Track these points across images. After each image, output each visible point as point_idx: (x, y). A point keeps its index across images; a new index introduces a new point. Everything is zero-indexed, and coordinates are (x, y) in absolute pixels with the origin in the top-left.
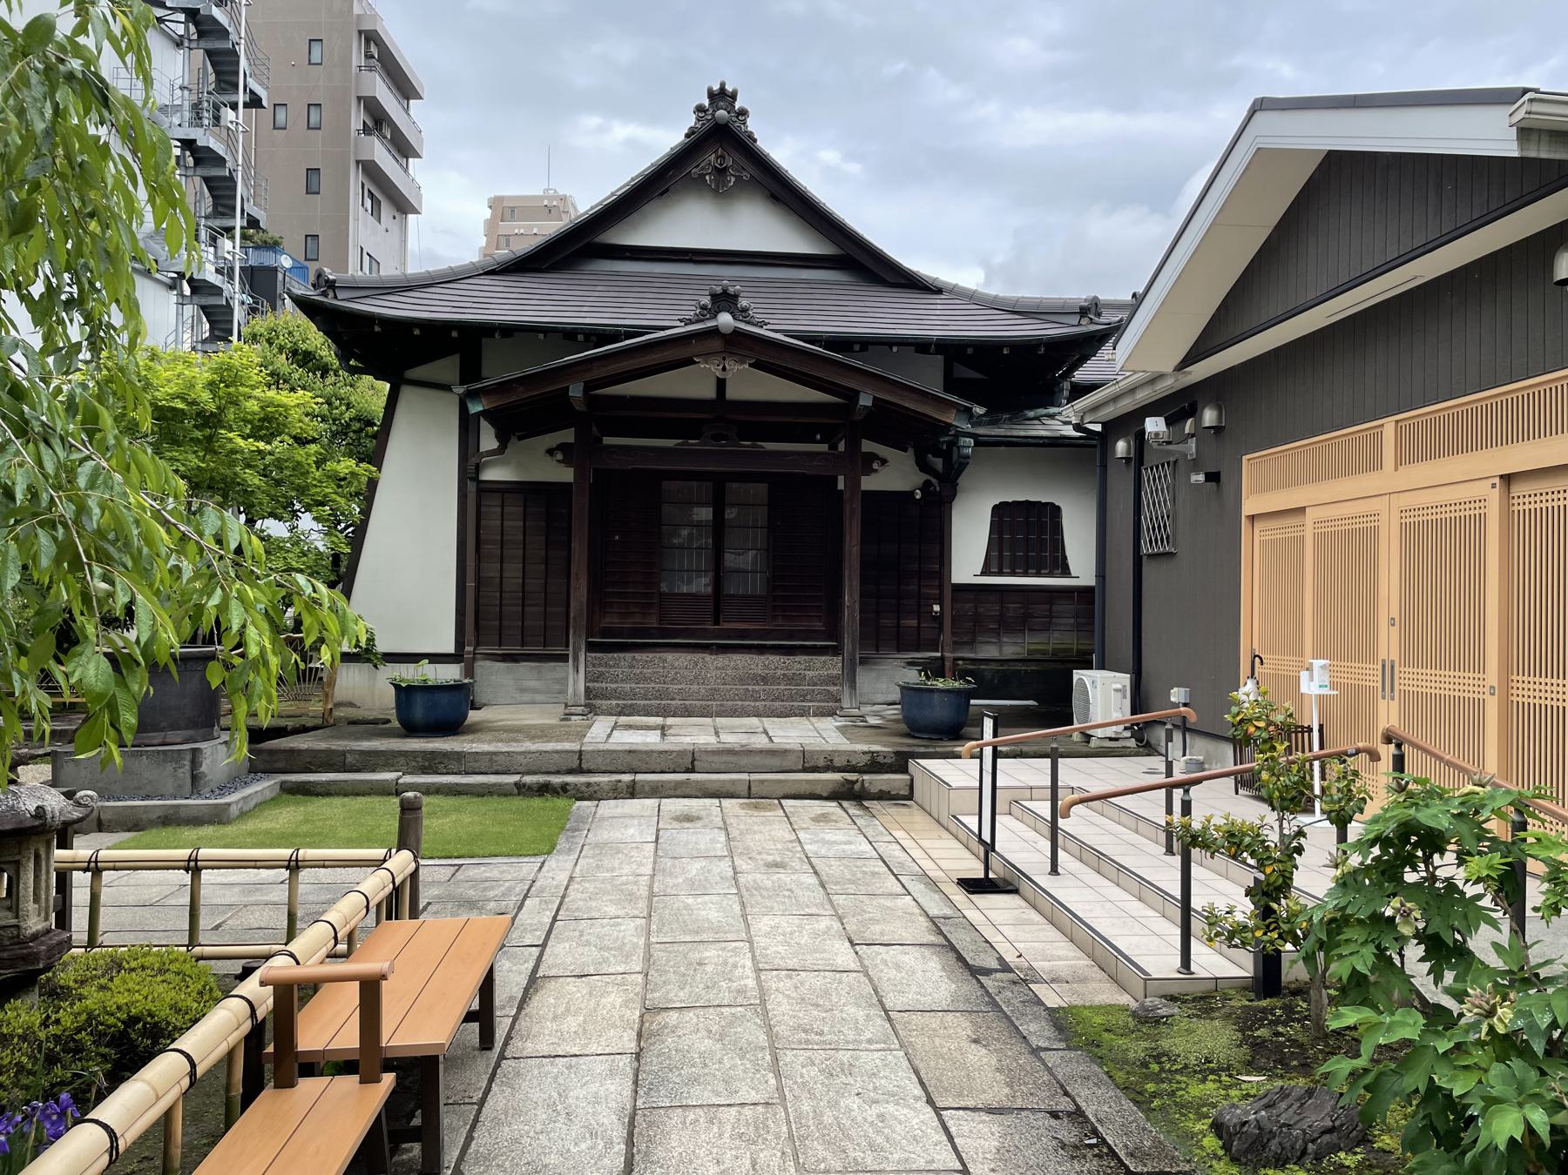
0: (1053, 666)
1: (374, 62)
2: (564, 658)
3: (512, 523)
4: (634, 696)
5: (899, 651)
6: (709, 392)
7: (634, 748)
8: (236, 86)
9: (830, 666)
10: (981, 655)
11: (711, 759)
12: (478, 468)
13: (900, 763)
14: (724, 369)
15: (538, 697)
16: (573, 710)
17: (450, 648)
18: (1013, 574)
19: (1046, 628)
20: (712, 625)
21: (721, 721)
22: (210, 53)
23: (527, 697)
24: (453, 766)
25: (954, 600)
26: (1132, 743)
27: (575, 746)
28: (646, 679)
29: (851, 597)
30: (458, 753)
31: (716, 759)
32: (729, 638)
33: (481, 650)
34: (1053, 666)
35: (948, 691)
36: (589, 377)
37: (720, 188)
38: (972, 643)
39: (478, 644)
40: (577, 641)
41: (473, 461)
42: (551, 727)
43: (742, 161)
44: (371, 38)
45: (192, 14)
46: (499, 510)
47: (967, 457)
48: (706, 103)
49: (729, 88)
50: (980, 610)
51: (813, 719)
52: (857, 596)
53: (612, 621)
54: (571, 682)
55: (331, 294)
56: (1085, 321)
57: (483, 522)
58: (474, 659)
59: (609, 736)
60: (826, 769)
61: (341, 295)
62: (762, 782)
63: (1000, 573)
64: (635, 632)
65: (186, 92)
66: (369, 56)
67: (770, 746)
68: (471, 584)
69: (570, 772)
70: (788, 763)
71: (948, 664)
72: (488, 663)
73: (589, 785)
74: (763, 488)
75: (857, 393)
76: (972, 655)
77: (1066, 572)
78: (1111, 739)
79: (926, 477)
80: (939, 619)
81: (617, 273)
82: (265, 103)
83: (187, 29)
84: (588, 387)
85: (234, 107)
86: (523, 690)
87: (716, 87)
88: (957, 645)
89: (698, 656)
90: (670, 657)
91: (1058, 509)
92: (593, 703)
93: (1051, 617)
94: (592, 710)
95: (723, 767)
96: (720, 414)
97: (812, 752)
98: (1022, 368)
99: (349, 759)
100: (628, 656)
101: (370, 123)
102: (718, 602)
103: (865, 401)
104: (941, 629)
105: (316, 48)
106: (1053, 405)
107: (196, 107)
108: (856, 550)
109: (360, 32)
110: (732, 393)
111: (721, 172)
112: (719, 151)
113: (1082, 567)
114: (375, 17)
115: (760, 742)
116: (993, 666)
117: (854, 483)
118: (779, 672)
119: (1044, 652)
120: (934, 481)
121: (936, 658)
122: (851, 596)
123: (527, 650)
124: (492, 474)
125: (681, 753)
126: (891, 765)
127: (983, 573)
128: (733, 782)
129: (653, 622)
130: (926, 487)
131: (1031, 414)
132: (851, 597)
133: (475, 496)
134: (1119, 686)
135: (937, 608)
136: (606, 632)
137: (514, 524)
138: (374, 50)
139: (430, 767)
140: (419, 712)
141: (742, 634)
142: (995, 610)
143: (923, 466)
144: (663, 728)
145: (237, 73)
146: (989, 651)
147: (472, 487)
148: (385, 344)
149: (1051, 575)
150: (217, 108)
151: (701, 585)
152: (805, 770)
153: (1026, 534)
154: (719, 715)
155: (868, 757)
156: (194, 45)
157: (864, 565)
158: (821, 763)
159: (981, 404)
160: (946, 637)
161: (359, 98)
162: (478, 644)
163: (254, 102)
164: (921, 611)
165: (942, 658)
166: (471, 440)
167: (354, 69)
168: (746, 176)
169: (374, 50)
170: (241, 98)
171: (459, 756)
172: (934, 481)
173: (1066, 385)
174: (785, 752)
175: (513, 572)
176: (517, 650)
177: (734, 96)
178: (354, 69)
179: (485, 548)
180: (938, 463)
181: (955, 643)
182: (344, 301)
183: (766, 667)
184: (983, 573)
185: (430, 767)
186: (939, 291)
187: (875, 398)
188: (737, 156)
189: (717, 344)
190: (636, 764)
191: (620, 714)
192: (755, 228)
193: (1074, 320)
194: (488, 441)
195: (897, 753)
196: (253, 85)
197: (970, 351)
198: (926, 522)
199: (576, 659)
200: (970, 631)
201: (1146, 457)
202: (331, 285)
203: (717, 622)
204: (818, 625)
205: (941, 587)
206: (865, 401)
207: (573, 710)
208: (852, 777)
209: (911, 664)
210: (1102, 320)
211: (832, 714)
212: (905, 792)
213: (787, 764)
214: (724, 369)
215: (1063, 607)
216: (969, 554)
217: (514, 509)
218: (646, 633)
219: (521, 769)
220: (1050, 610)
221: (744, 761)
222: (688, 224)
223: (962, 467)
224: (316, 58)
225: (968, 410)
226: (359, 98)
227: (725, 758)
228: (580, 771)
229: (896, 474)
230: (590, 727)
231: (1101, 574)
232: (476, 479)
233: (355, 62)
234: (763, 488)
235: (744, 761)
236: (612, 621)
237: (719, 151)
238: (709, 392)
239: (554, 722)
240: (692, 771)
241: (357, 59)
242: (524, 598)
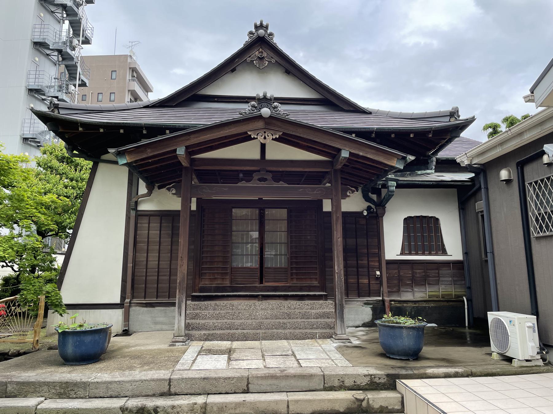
0: (442, 304)
1: (134, 78)
2: (173, 304)
3: (154, 232)
4: (215, 328)
5: (359, 296)
6: (257, 156)
7: (207, 375)
8: (76, 78)
9: (327, 306)
10: (404, 298)
11: (260, 382)
12: (136, 203)
13: (390, 384)
14: (265, 138)
15: (164, 327)
16: (178, 339)
17: (118, 300)
18: (417, 254)
19: (437, 283)
20: (259, 283)
21: (266, 344)
22: (67, 66)
23: (158, 327)
24: (81, 393)
25: (387, 269)
26: (541, 363)
27: (163, 374)
28: (223, 317)
29: (338, 266)
30: (84, 383)
31: (264, 382)
32: (268, 291)
33: (135, 301)
34: (442, 304)
35: (412, 328)
36: (188, 143)
37: (260, 68)
38: (398, 291)
39: (133, 297)
40: (179, 296)
41: (134, 200)
42: (160, 352)
43: (272, 54)
44: (134, 70)
45: (60, 51)
46: (147, 225)
47: (393, 191)
48: (254, 31)
49: (265, 24)
50: (401, 274)
51: (319, 341)
52: (342, 266)
53: (205, 283)
54: (176, 321)
55: (56, 111)
56: (452, 119)
57: (138, 232)
58: (130, 306)
59: (194, 361)
60: (342, 387)
61: (62, 112)
62: (297, 401)
63: (410, 254)
64: (217, 289)
65: (56, 80)
66: (133, 76)
67: (299, 371)
68: (130, 265)
69: (162, 395)
70: (314, 384)
71: (387, 304)
72: (138, 308)
73: (173, 407)
74: (283, 213)
75: (339, 150)
76: (399, 299)
77: (444, 252)
78: (527, 361)
79: (368, 204)
80: (379, 279)
81: (211, 108)
82: (87, 85)
83: (58, 58)
84: (191, 151)
85: (75, 86)
86: (156, 323)
87: (258, 23)
88: (390, 293)
89: (251, 302)
90: (236, 302)
91: (437, 220)
92: (189, 334)
93: (439, 277)
94: (189, 338)
95: (269, 389)
96: (263, 167)
97: (330, 376)
98: (424, 141)
99: (10, 388)
100: (213, 303)
101: (133, 99)
102: (262, 271)
103: (345, 154)
104: (381, 284)
105: (114, 74)
106: (428, 169)
107: (60, 87)
108: (340, 240)
109: (130, 68)
110: (269, 156)
111: (261, 59)
112: (260, 51)
113: (454, 249)
114: (135, 63)
115: (291, 366)
116: (410, 304)
117: (336, 205)
118: (297, 311)
119: (437, 296)
120: (373, 206)
121: (380, 301)
122: (338, 266)
123: (160, 300)
124: (145, 206)
125: (240, 379)
126: (384, 384)
127: (402, 254)
128: (277, 402)
129: (227, 283)
130: (369, 209)
131: (419, 172)
132: (338, 266)
133: (135, 217)
134: (531, 325)
135: (378, 273)
136: (202, 290)
137: (155, 233)
138: (135, 74)
139: (65, 393)
140: (70, 349)
141: (275, 289)
142: (409, 273)
143: (366, 198)
144: (229, 352)
145: (76, 74)
146: (407, 296)
147: (133, 213)
148: (87, 140)
149: (436, 254)
150: (67, 85)
151: (251, 263)
152: (325, 389)
153: (421, 232)
154: (265, 339)
155: (368, 379)
156: (60, 63)
157: (346, 250)
158: (336, 384)
159: (412, 155)
160: (385, 288)
161: (129, 91)
162: (133, 297)
163: (83, 84)
164: (370, 275)
165: (383, 301)
166: (134, 189)
167: (127, 81)
168: (273, 61)
169: (135, 74)
170: (77, 82)
171: (85, 385)
172: (373, 206)
173: (434, 159)
174: (311, 377)
175: (153, 257)
176: (154, 300)
177: (267, 27)
178: (127, 81)
179: (139, 245)
180: (374, 197)
181: (389, 292)
182: (63, 114)
183: (289, 308)
184: (402, 254)
185: (65, 393)
186: (370, 113)
187: (350, 153)
188: (269, 52)
189: (260, 124)
190: (208, 388)
191: (206, 340)
192: (279, 86)
193: (447, 119)
194: (143, 189)
195: (388, 375)
196: (82, 77)
197: (393, 136)
198: (366, 229)
199: (180, 307)
200: (397, 285)
201: (526, 177)
202: (56, 107)
203: (261, 282)
204: (315, 283)
205: (380, 261)
206: (345, 154)
207: (178, 339)
208: (359, 394)
209: (367, 304)
210: (460, 118)
211: (330, 337)
212: (398, 407)
213: (313, 385)
214: (265, 138)
215: (444, 271)
216: (393, 245)
217: (155, 225)
218: (224, 289)
219: (128, 394)
220: (438, 273)
221: (283, 384)
222: (246, 85)
223: (390, 196)
224: (114, 77)
225: (404, 158)
226: (129, 91)
227: (270, 382)
228: (168, 394)
229: (354, 203)
230: (184, 352)
231: (466, 253)
232: (135, 209)
233: (128, 78)
234: (283, 213)
235: (283, 384)
236: (205, 283)
237: (260, 51)
238: (257, 156)
239: (165, 346)
240: (247, 391)
241: (129, 77)
242: (158, 272)
